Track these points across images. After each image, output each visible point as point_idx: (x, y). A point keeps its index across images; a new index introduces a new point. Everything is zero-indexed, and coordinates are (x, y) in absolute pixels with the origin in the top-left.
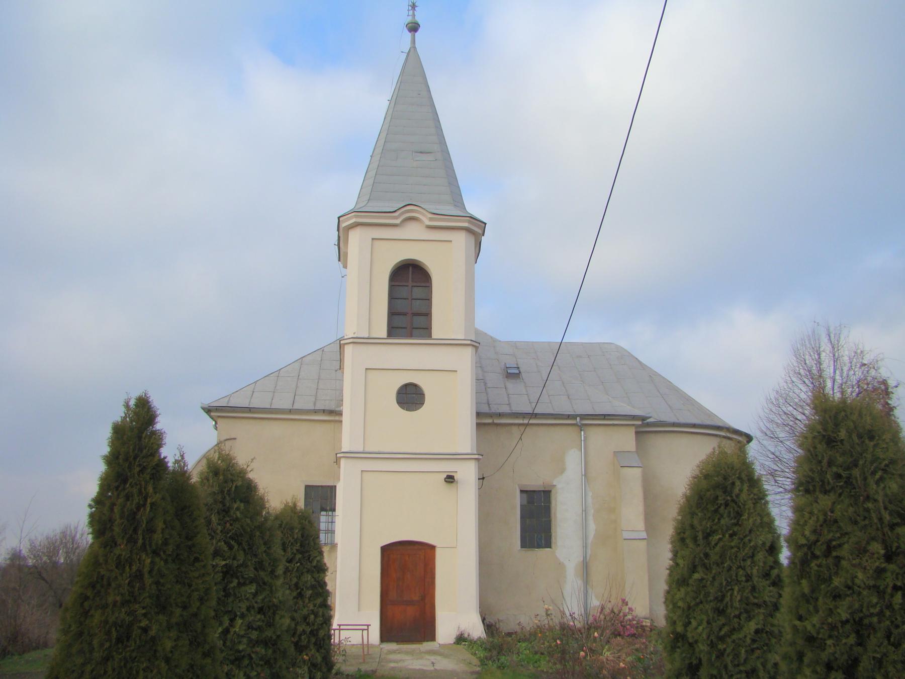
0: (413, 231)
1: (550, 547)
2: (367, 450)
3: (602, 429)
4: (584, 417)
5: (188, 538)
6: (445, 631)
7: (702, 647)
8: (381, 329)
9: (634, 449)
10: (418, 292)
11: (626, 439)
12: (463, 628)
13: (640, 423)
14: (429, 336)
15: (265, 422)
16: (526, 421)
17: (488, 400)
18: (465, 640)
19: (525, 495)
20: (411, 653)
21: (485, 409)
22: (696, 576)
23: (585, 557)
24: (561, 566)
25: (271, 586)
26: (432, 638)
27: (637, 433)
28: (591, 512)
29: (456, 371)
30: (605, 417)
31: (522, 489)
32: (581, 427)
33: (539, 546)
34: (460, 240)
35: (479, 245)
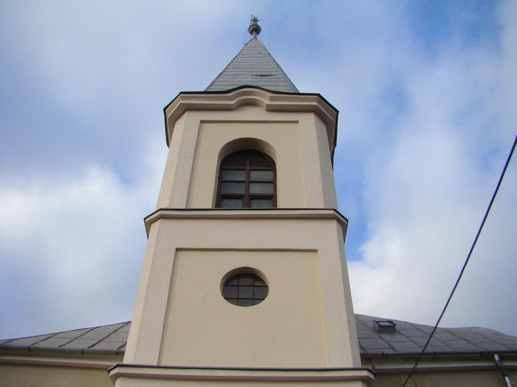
15: (49, 372)
29: (315, 251)
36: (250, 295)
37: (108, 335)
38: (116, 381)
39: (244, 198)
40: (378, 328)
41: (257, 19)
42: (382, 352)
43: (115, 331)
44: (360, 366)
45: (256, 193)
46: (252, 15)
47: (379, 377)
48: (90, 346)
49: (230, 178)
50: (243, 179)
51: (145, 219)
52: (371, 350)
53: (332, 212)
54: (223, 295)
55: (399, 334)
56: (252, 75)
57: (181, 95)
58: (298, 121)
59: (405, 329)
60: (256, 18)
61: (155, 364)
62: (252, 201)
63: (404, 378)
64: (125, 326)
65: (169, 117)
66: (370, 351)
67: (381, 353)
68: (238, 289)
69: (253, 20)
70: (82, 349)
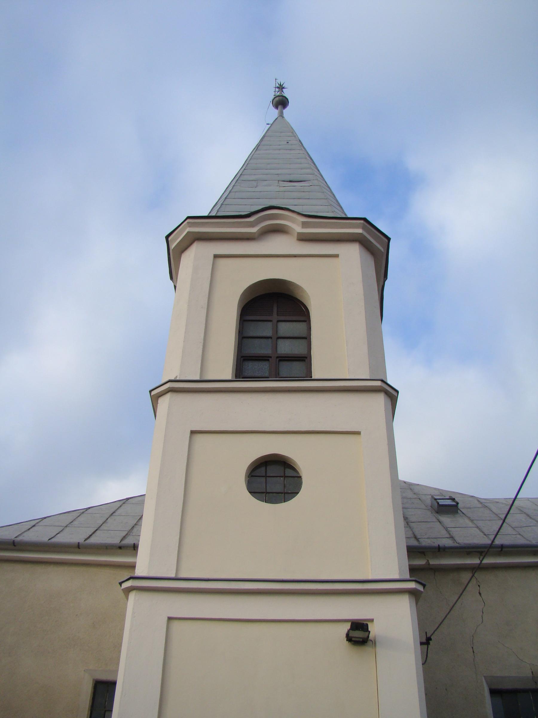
15: (39, 569)
17: (413, 533)
29: (358, 433)
31: (493, 687)
36: (278, 488)
37: (104, 519)
38: (129, 594)
39: (270, 359)
40: (437, 508)
41: (283, 86)
42: (439, 545)
43: (113, 513)
44: (407, 576)
45: (285, 353)
46: (276, 79)
47: (435, 574)
48: (86, 537)
49: (251, 334)
50: (269, 333)
51: (151, 391)
52: (426, 540)
53: (379, 383)
54: (247, 490)
55: (462, 515)
56: (278, 181)
57: (188, 221)
58: (338, 255)
59: (470, 508)
60: (282, 84)
61: (173, 575)
62: (282, 363)
63: (465, 576)
64: (124, 505)
65: (172, 248)
66: (426, 542)
67: (438, 545)
68: (266, 480)
69: (278, 88)
70: (77, 543)
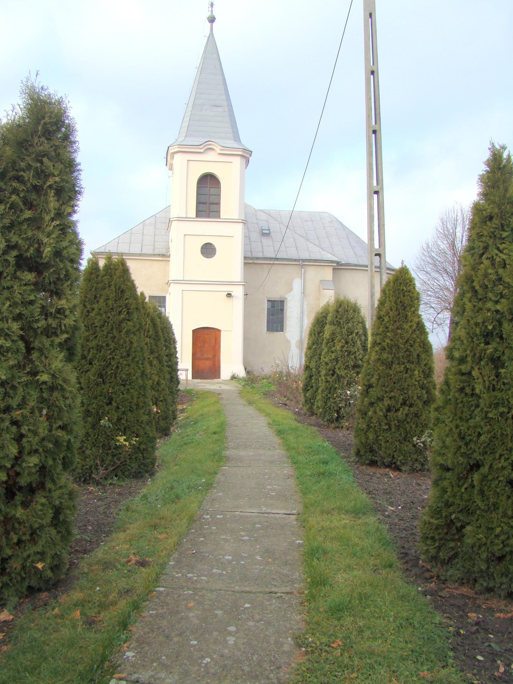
0: (211, 156)
1: (283, 331)
2: (185, 279)
3: (314, 267)
4: (304, 260)
5: (156, 333)
6: (225, 373)
7: (314, 370)
8: (192, 213)
9: (331, 279)
10: (213, 191)
11: (328, 274)
12: (234, 372)
13: (336, 265)
14: (219, 217)
16: (272, 262)
18: (235, 378)
19: (270, 303)
20: (209, 383)
21: (249, 255)
22: (314, 347)
23: (301, 337)
24: (288, 342)
25: (170, 348)
26: (219, 377)
27: (333, 269)
28: (306, 313)
30: (316, 261)
32: (303, 266)
33: (277, 331)
34: (237, 161)
35: (248, 161)
